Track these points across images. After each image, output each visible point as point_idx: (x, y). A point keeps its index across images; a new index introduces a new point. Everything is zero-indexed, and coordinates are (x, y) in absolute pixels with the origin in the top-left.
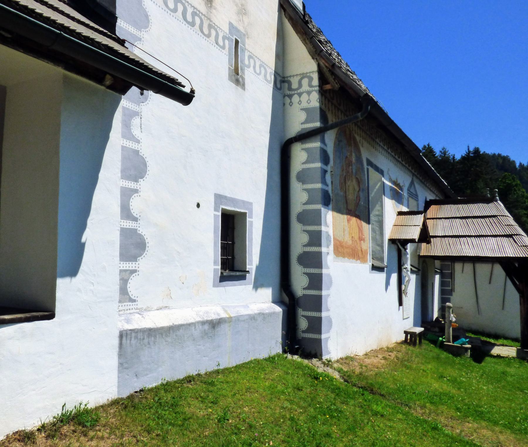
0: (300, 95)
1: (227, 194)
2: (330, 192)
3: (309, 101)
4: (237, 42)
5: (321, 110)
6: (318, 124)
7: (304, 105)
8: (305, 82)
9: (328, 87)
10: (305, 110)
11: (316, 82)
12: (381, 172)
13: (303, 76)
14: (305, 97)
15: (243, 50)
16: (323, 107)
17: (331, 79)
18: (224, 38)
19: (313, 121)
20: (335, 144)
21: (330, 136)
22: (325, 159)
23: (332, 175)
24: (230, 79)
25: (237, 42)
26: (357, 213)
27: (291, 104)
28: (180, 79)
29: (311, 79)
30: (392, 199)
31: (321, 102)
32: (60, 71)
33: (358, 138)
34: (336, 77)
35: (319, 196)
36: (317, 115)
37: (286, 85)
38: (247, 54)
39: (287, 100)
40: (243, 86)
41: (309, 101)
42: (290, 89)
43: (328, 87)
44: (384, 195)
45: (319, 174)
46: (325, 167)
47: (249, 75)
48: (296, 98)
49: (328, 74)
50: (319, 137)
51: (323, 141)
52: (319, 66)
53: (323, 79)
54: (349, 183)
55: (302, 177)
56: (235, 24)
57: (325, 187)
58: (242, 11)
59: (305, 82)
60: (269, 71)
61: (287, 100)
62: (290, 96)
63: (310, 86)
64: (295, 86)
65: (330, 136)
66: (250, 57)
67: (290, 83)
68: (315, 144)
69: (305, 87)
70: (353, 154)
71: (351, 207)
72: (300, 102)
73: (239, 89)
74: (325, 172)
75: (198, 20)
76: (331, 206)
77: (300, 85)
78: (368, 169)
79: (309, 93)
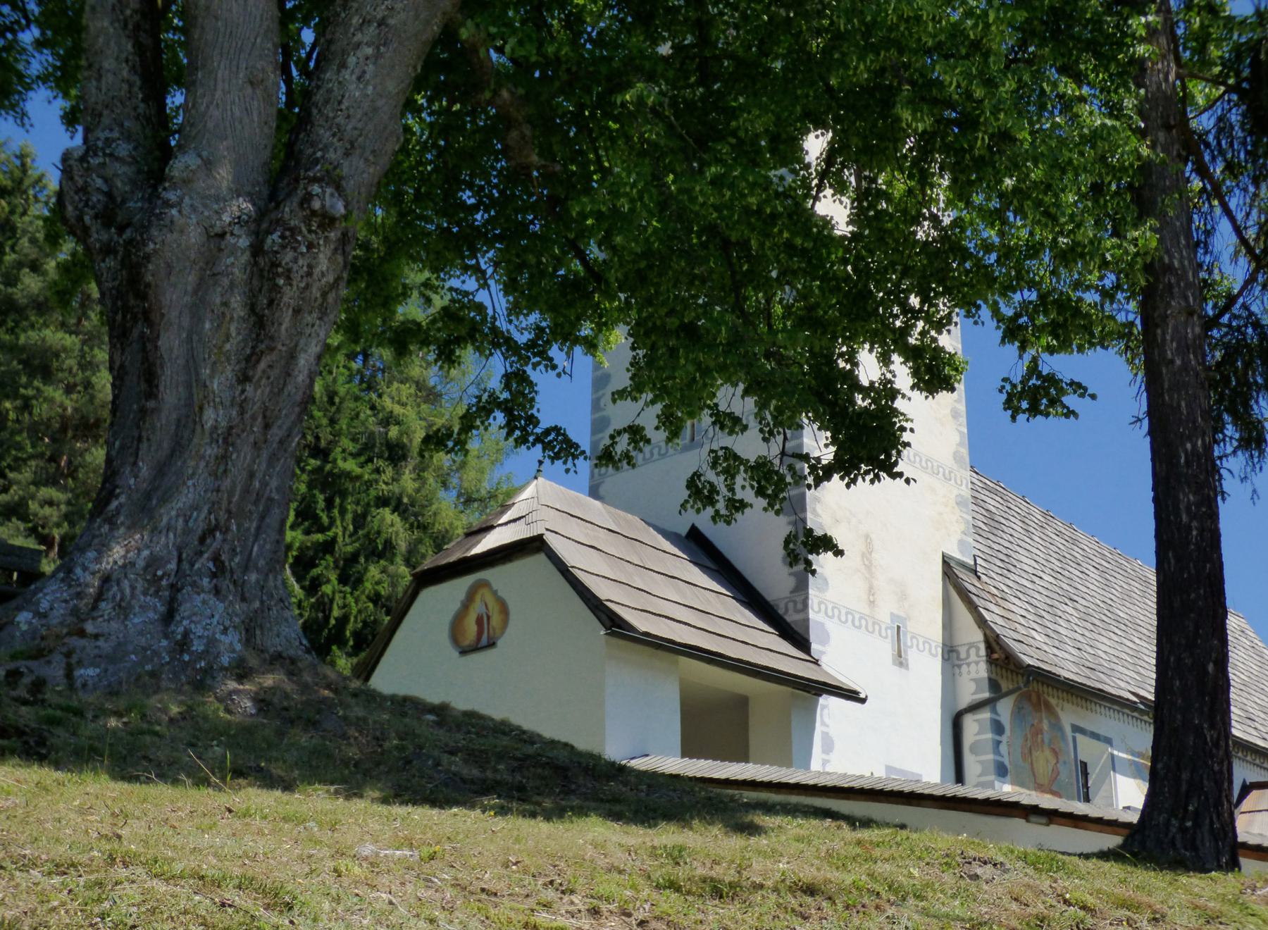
0: (968, 665)
1: (897, 765)
2: (1007, 763)
3: (977, 672)
4: (899, 628)
5: (990, 680)
6: (986, 695)
7: (973, 675)
8: (973, 651)
9: (996, 656)
10: (973, 680)
11: (983, 652)
12: (1109, 741)
13: (971, 645)
14: (973, 666)
15: (905, 634)
16: (994, 676)
17: (997, 648)
18: (886, 629)
19: (983, 692)
20: (1013, 712)
21: (1005, 708)
22: (998, 728)
23: (1009, 746)
24: (894, 663)
25: (899, 628)
26: (1054, 788)
27: (960, 674)
28: (858, 689)
29: (978, 649)
30: (1135, 778)
31: (990, 671)
32: (790, 689)
33: (1053, 701)
34: (1001, 647)
35: (992, 768)
36: (986, 684)
37: (955, 655)
38: (909, 636)
39: (957, 671)
40: (907, 667)
41: (977, 672)
42: (958, 658)
43: (996, 656)
44: (1114, 770)
45: (990, 746)
46: (998, 738)
47: (912, 656)
48: (964, 668)
49: (994, 644)
50: (988, 708)
51: (994, 711)
52: (985, 635)
53: (990, 648)
54: (1036, 754)
55: (974, 750)
56: (896, 612)
57: (999, 758)
58: (903, 596)
59: (973, 651)
60: (934, 645)
61: (957, 671)
62: (959, 666)
63: (978, 656)
64: (963, 655)
65: (1005, 708)
66: (912, 638)
67: (958, 653)
68: (985, 715)
69: (973, 657)
70: (1045, 721)
71: (1044, 780)
72: (969, 672)
73: (903, 670)
74: (999, 743)
75: (863, 622)
76: (1008, 778)
77: (968, 656)
78: (1074, 739)
79: (977, 663)
